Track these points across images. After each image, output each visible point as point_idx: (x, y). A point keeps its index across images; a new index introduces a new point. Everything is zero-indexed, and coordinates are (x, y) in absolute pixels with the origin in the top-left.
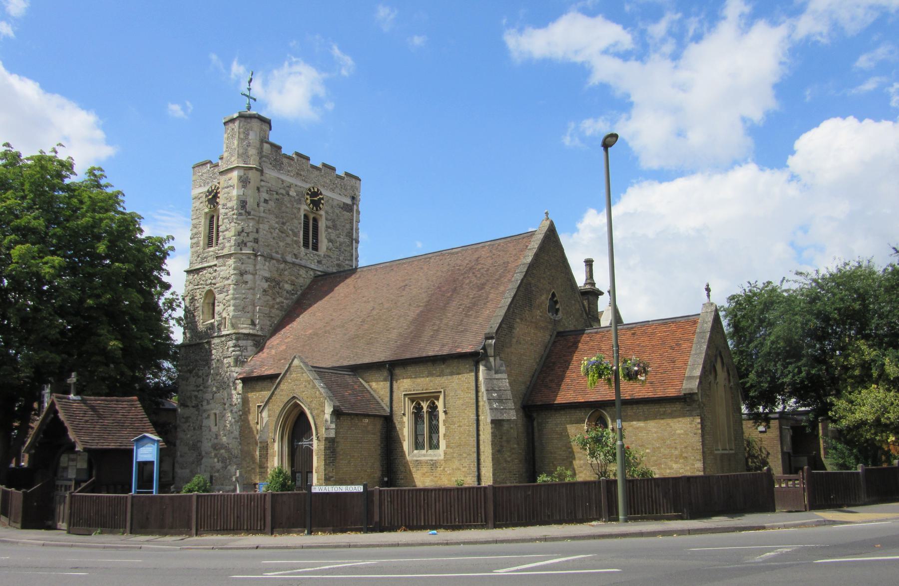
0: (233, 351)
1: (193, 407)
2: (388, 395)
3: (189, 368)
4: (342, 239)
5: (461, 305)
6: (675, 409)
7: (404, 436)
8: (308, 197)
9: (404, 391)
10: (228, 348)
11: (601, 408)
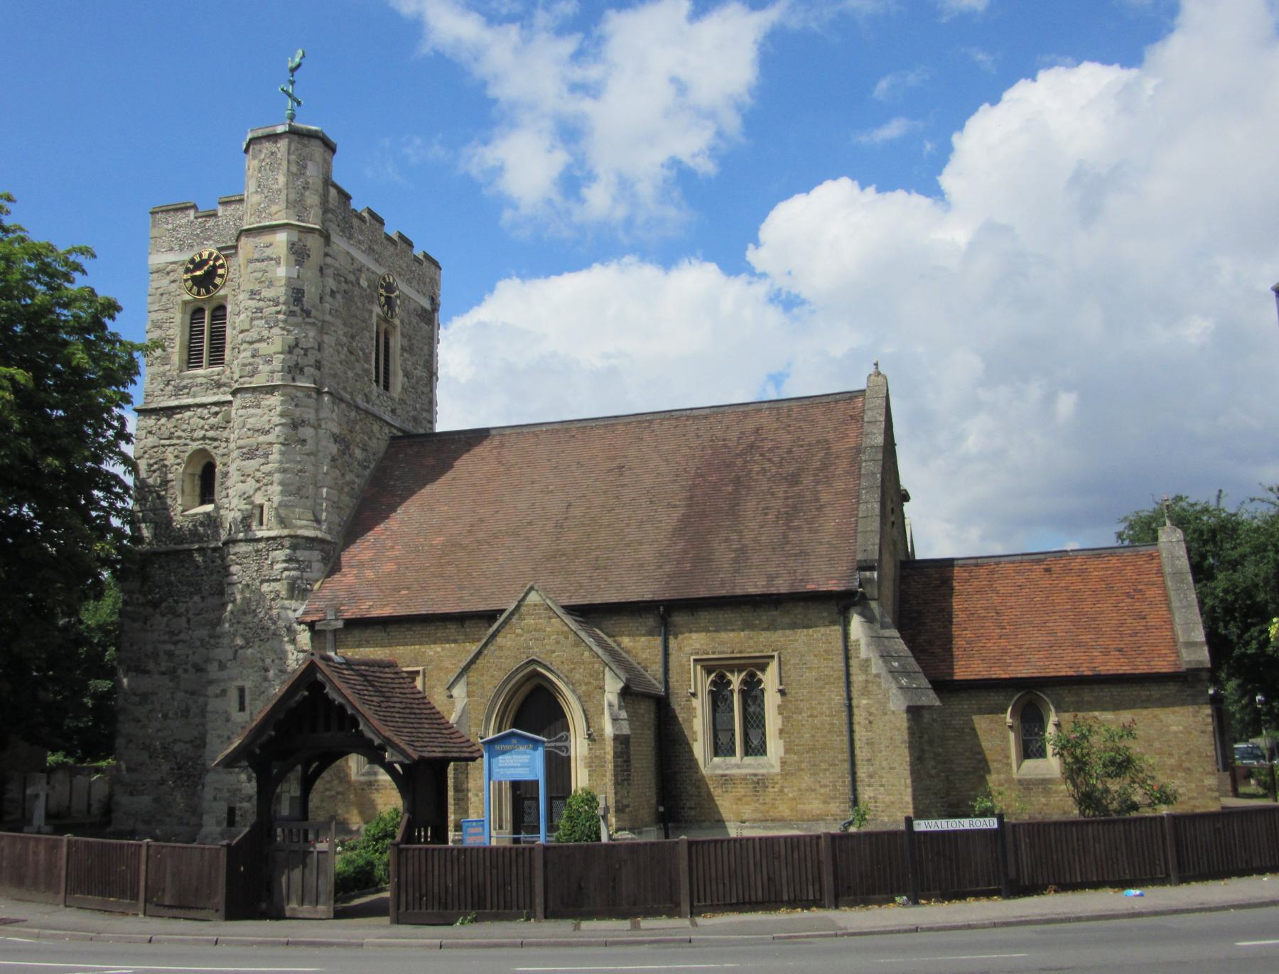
0: (286, 569)
2: (660, 658)
6: (1167, 692)
7: (694, 733)
9: (692, 654)
10: (272, 564)
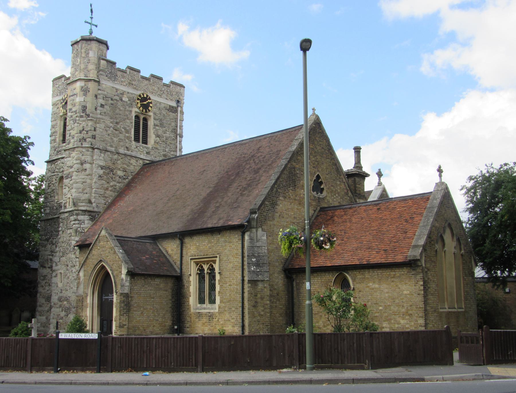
1: (49, 268)
3: (46, 237)
4: (168, 134)
5: (239, 186)
7: (190, 293)
8: (139, 101)
9: (190, 256)
11: (345, 272)
